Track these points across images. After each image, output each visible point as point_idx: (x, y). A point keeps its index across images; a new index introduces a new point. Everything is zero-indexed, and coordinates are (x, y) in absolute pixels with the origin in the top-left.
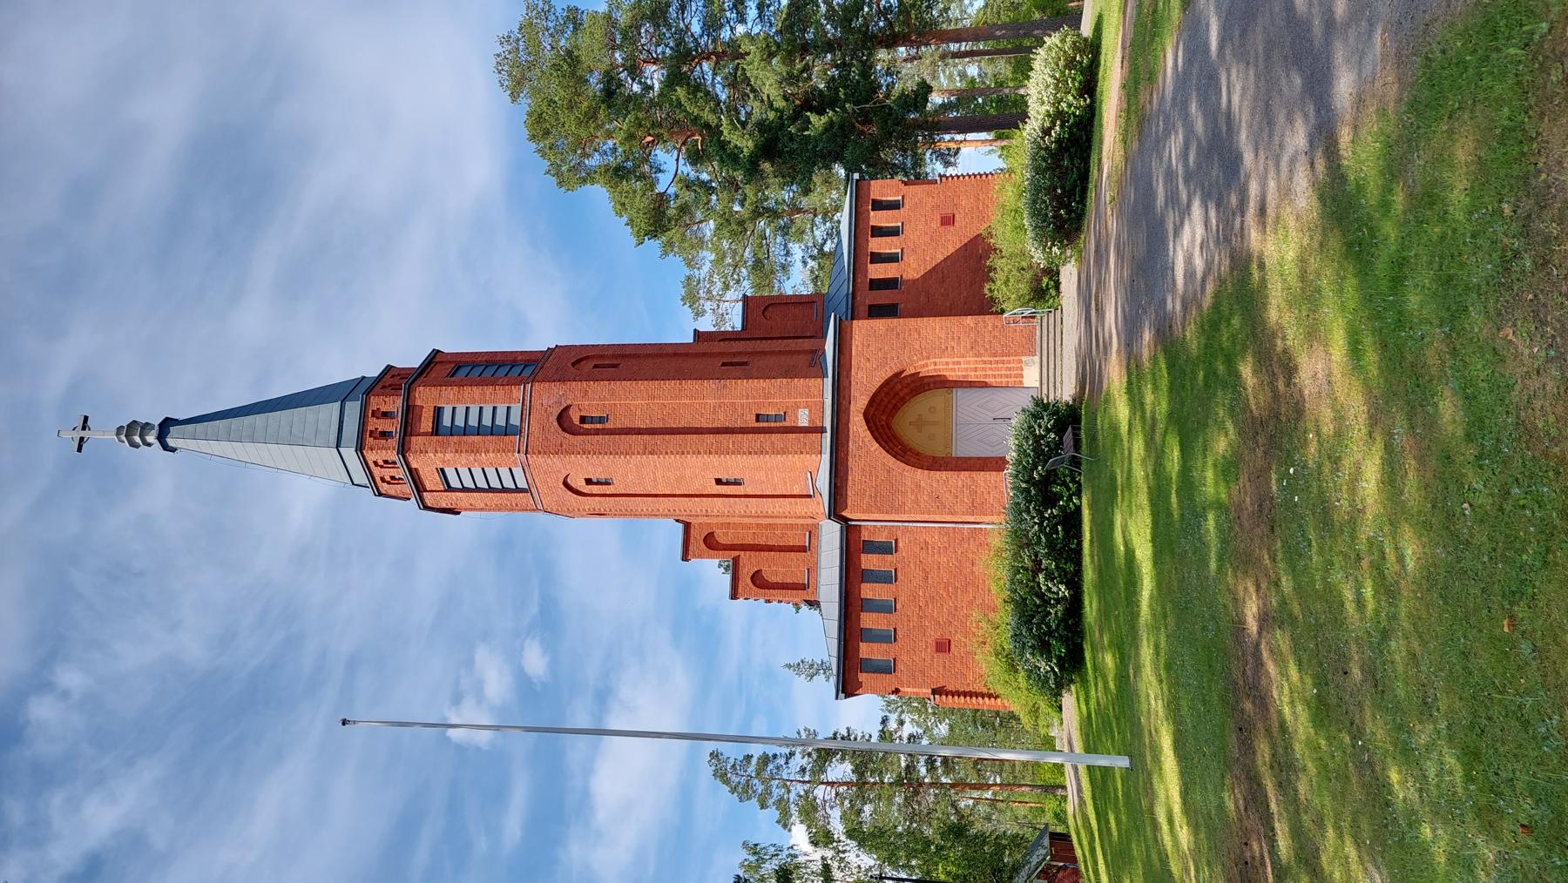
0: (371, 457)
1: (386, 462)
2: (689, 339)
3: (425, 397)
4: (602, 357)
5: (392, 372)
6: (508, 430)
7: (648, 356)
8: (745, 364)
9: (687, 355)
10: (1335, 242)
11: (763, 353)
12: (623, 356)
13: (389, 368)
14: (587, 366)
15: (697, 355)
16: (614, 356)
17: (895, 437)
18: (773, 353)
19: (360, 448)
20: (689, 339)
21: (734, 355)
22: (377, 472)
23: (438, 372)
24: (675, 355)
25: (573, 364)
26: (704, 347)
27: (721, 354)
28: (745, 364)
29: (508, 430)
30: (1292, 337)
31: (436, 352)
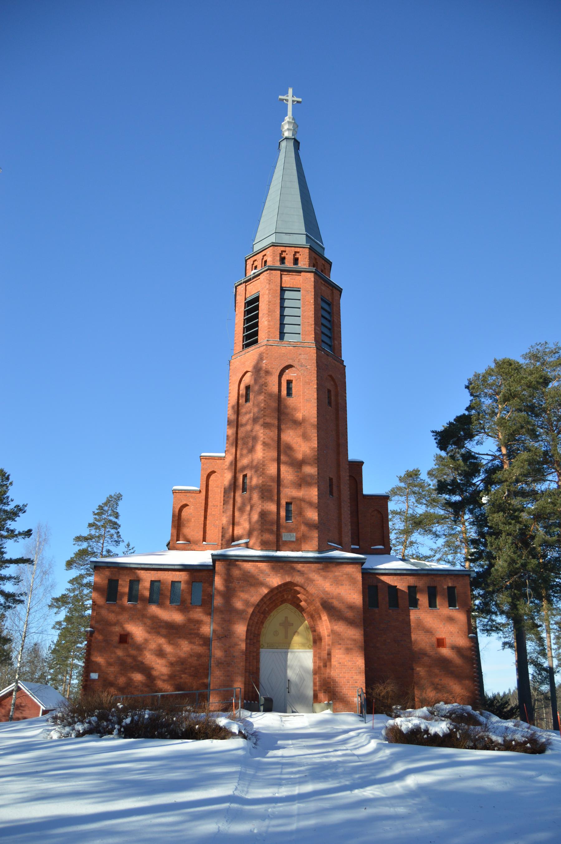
0: (268, 252)
1: (266, 262)
2: (353, 455)
3: (306, 282)
4: (337, 395)
5: (327, 266)
6: (282, 335)
7: (337, 426)
8: (331, 493)
9: (338, 454)
10: (260, 523)
11: (340, 507)
12: (337, 410)
13: (330, 264)
14: (329, 385)
15: (338, 465)
16: (337, 404)
17: (276, 606)
18: (340, 514)
19: (273, 245)
20: (353, 455)
21: (339, 487)
22: (260, 256)
23: (326, 292)
24: (338, 445)
25: (331, 376)
26: (345, 475)
27: (339, 477)
28: (331, 493)
29: (282, 335)
30: (478, 563)
31: (340, 291)
